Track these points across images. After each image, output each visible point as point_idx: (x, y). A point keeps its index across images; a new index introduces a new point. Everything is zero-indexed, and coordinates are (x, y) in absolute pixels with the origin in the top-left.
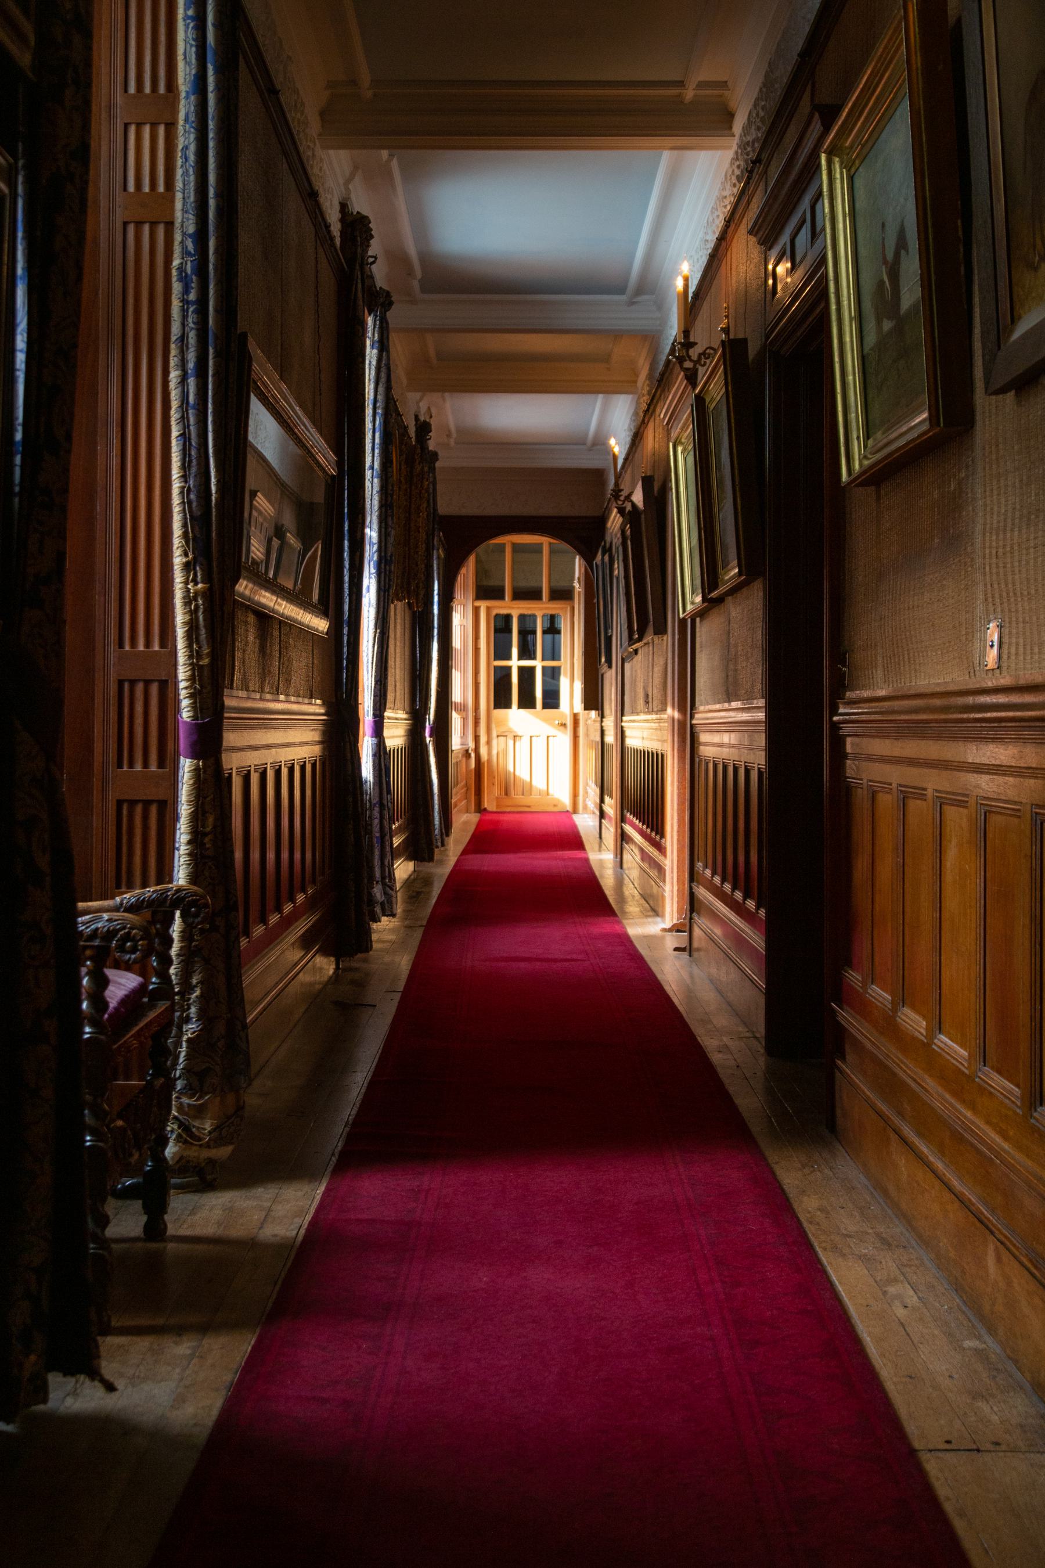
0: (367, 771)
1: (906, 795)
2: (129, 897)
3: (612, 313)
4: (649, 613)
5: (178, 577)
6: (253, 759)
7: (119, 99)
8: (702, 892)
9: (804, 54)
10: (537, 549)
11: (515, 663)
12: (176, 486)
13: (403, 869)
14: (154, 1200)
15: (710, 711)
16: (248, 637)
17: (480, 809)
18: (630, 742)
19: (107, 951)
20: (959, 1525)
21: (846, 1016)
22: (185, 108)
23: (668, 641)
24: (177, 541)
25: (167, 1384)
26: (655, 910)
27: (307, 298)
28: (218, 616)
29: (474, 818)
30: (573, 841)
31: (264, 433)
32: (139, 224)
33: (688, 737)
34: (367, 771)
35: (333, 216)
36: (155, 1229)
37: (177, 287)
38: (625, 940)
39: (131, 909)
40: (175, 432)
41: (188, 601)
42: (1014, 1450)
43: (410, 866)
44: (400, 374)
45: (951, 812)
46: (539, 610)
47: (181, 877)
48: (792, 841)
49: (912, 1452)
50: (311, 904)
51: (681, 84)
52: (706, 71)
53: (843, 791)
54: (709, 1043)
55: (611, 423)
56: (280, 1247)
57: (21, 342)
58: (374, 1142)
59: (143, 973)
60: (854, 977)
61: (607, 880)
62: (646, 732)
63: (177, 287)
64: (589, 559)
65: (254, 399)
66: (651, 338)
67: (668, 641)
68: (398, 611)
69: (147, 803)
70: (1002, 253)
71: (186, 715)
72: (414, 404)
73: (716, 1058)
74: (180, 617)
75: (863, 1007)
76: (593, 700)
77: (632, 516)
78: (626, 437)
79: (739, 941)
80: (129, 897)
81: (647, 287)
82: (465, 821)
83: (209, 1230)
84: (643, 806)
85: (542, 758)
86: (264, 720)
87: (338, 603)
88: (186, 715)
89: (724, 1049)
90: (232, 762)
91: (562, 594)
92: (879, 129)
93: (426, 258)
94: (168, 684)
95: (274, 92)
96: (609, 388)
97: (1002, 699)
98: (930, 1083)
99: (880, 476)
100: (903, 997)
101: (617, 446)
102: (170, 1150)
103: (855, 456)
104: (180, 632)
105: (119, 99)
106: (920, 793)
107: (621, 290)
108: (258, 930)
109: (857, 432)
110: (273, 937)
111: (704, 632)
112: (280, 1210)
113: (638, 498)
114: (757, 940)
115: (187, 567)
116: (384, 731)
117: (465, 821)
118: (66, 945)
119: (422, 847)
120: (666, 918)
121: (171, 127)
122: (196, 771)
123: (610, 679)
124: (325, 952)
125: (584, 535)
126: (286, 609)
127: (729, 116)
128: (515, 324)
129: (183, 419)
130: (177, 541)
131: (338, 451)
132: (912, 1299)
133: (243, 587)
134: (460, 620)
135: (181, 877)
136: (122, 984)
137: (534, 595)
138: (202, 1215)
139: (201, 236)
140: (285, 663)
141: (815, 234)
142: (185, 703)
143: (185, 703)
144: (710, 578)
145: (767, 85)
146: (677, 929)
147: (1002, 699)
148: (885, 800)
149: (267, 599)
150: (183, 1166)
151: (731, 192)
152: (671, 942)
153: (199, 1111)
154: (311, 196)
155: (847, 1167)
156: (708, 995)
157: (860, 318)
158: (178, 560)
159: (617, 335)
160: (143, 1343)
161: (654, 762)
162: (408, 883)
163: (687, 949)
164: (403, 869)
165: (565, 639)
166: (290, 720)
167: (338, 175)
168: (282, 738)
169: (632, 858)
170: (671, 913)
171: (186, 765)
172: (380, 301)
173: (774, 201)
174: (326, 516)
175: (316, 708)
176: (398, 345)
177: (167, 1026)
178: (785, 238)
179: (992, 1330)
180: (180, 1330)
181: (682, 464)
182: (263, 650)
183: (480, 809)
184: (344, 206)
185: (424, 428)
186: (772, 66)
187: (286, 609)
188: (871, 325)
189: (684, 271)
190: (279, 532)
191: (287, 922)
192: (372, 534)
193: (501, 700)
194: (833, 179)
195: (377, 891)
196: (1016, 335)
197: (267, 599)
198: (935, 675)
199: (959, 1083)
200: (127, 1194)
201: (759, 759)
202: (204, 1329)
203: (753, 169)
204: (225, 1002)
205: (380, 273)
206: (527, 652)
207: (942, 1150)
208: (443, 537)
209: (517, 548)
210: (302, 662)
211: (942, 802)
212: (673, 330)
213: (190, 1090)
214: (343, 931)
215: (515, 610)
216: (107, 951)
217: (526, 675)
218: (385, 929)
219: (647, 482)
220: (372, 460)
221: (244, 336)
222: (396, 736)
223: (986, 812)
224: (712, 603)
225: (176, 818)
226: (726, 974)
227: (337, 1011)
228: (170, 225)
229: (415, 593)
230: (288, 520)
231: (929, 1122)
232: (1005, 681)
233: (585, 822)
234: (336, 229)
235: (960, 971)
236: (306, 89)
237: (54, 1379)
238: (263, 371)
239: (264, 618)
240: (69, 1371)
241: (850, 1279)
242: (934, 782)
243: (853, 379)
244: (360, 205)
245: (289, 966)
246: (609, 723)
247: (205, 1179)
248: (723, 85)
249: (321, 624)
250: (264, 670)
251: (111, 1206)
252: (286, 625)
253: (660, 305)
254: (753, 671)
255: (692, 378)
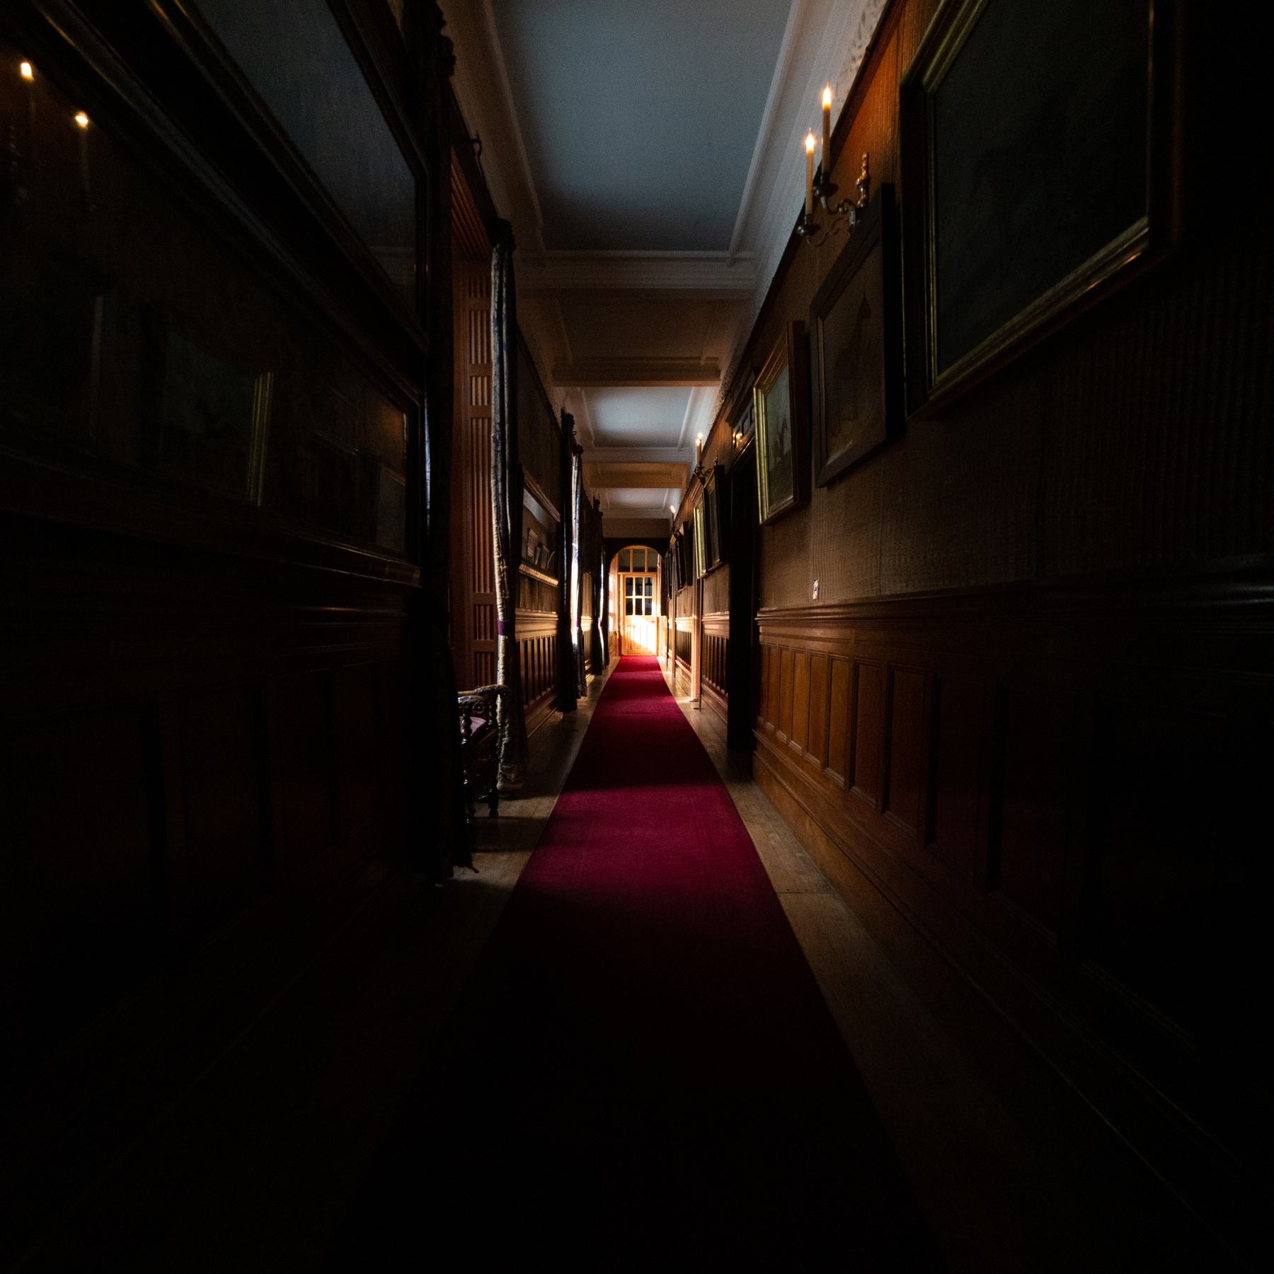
0: (575, 640)
1: (782, 649)
2: (479, 689)
3: (672, 455)
4: (686, 577)
5: (496, 564)
6: (528, 636)
7: (468, 366)
8: (705, 687)
9: (748, 346)
10: (643, 551)
11: (634, 597)
12: (494, 527)
13: (589, 678)
14: (493, 802)
15: (708, 616)
16: (526, 587)
17: (620, 655)
18: (679, 628)
19: (470, 710)
20: (791, 920)
21: (757, 734)
22: (495, 369)
23: (693, 588)
24: (495, 549)
25: (498, 870)
26: (687, 694)
27: (547, 448)
28: (513, 581)
29: (618, 658)
30: (657, 667)
31: (531, 504)
32: (477, 419)
33: (700, 626)
34: (575, 640)
35: (558, 415)
36: (494, 813)
37: (493, 445)
38: (675, 706)
39: (480, 694)
40: (493, 505)
41: (500, 573)
42: (813, 892)
43: (593, 677)
44: (587, 480)
45: (798, 655)
46: (644, 576)
47: (500, 682)
48: (737, 666)
49: (775, 893)
50: (552, 692)
51: (699, 358)
52: (710, 353)
53: (758, 647)
54: (706, 744)
55: (671, 501)
56: (540, 821)
57: (428, 468)
58: (577, 782)
59: (487, 718)
60: (761, 719)
61: (669, 683)
62: (685, 624)
63: (493, 445)
64: (663, 555)
65: (526, 492)
66: (687, 465)
67: (693, 588)
68: (587, 576)
69: (486, 653)
70: (824, 428)
71: (500, 618)
72: (593, 493)
73: (709, 750)
74: (497, 580)
75: (763, 730)
76: (665, 611)
77: (679, 538)
78: (678, 506)
79: (718, 704)
80: (479, 689)
81: (686, 444)
82: (614, 659)
83: (514, 815)
84: (683, 653)
85: (645, 634)
86: (533, 620)
87: (560, 571)
88: (500, 618)
89: (712, 746)
90: (520, 637)
91: (653, 569)
92: (776, 379)
93: (597, 432)
94: (493, 606)
95: (532, 363)
96: (670, 486)
97: (823, 611)
98: (788, 759)
99: (775, 521)
100: (779, 726)
101: (674, 509)
102: (499, 785)
103: (765, 513)
104: (497, 586)
105: (468, 366)
106: (787, 648)
107: (675, 445)
108: (532, 702)
109: (766, 503)
110: (538, 704)
111: (706, 584)
112: (541, 807)
113: (682, 531)
114: (725, 705)
115: (499, 559)
116: (581, 625)
117: (614, 659)
118: (456, 710)
119: (597, 669)
120: (689, 694)
121: (489, 378)
122: (505, 641)
123: (671, 602)
124: (559, 710)
125: (660, 545)
126: (540, 576)
127: (718, 372)
128: (633, 459)
129: (497, 500)
130: (495, 549)
131: (561, 512)
132: (777, 838)
133: (522, 567)
134: (612, 580)
135: (500, 682)
136: (477, 723)
137: (642, 570)
138: (511, 809)
139: (502, 424)
140: (541, 599)
141: (752, 422)
142: (500, 614)
143: (500, 614)
144: (709, 563)
145: (734, 357)
146: (695, 701)
147: (823, 611)
148: (773, 650)
149: (533, 572)
150: (503, 790)
151: (719, 404)
152: (693, 706)
153: (509, 771)
154: (549, 407)
155: (756, 791)
156: (706, 725)
157: (768, 456)
158: (496, 557)
159: (673, 464)
160: (490, 856)
161: (687, 636)
162: (592, 684)
163: (699, 709)
164: (589, 678)
165: (654, 587)
166: (544, 620)
167: (560, 398)
168: (542, 628)
169: (679, 673)
170: (694, 694)
171: (501, 638)
172: (578, 451)
173: (735, 409)
174: (557, 538)
175: (554, 615)
176: (585, 467)
177: (495, 738)
178: (740, 424)
179: (806, 848)
180: (503, 851)
181: (698, 516)
182: (532, 593)
183: (620, 655)
184: (563, 411)
185: (597, 502)
186: (736, 350)
187: (540, 576)
188: (772, 462)
189: (700, 438)
190: (540, 545)
191: (543, 699)
192: (575, 545)
193: (629, 612)
194: (758, 399)
195: (580, 687)
196: (831, 461)
197: (533, 572)
198: (794, 601)
199: (798, 759)
200: (483, 801)
201: (726, 635)
202: (511, 850)
203: (728, 394)
204: (518, 731)
205: (578, 438)
206: (639, 592)
207: (791, 784)
208: (603, 549)
209: (635, 551)
210: (548, 597)
211: (795, 652)
212: (696, 463)
213: (505, 762)
214: (566, 702)
215: (634, 576)
216: (470, 710)
217: (639, 602)
218: (582, 701)
219: (685, 524)
220: (575, 515)
221: (520, 466)
222: (586, 626)
223: (812, 655)
224: (709, 573)
225: (497, 658)
226: (713, 719)
227: (565, 731)
228: (490, 419)
229: (590, 567)
230: (544, 541)
231: (786, 773)
232: (820, 604)
233: (661, 660)
234: (559, 420)
235: (800, 718)
236: (546, 360)
237: (455, 868)
238: (528, 478)
239: (532, 581)
240: (461, 866)
241: (755, 832)
242: (792, 644)
243: (765, 482)
244: (569, 411)
245: (547, 715)
246: (671, 621)
247: (512, 795)
248: (716, 359)
249: (555, 582)
250: (532, 601)
251: (476, 806)
252: (541, 583)
253: (691, 451)
254: (725, 600)
255: (703, 481)
